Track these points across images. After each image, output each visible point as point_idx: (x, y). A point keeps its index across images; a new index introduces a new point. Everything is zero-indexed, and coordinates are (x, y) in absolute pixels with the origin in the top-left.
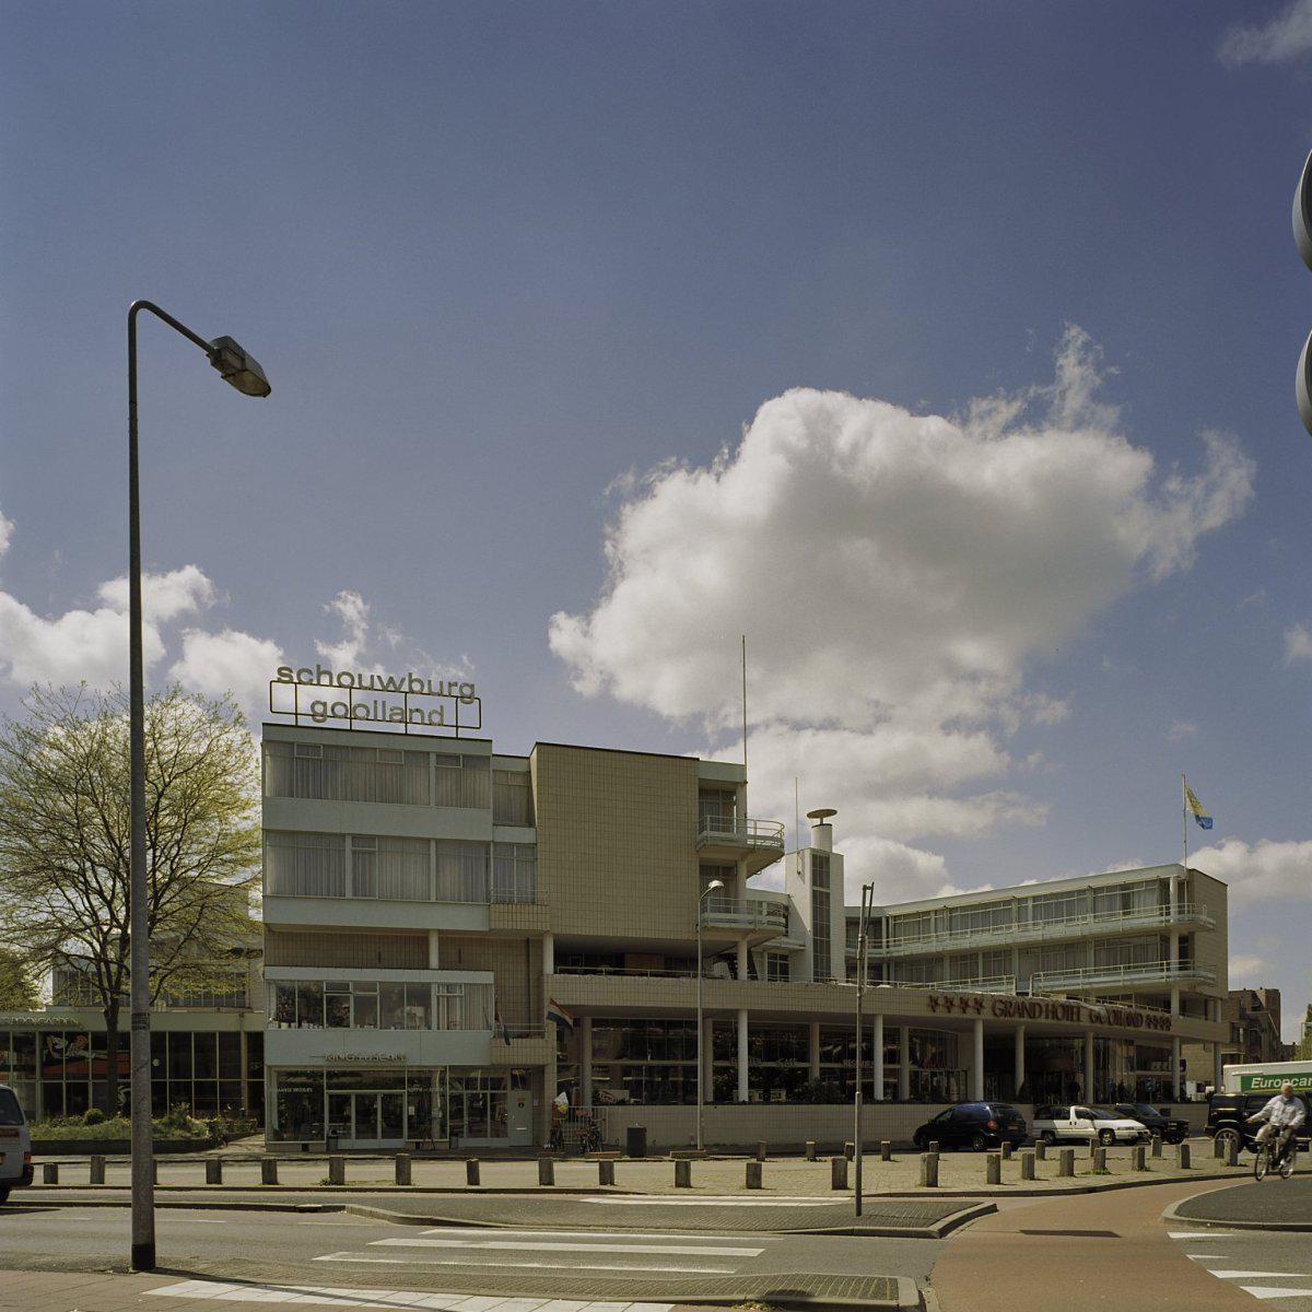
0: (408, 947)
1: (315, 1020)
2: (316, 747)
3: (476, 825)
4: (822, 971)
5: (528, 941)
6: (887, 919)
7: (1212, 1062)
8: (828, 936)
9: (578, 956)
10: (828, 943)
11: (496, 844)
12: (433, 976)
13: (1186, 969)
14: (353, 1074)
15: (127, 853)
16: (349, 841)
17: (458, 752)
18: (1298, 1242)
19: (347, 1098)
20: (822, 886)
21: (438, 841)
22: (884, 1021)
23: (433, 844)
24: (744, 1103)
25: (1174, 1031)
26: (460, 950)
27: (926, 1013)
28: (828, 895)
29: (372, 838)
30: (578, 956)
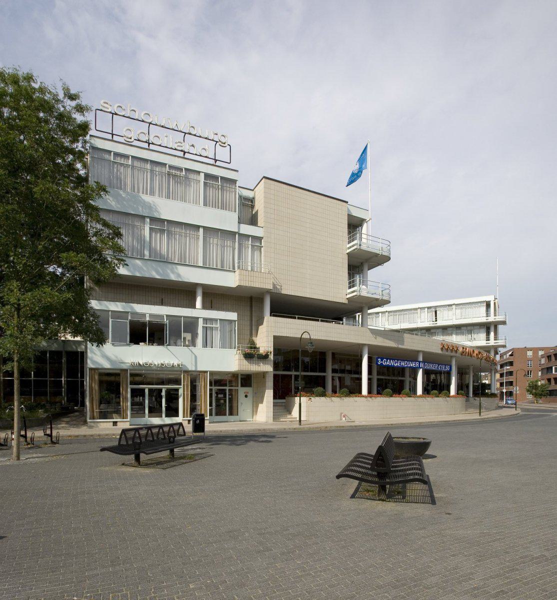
0: (183, 293)
3: (228, 220)
9: (286, 307)
11: (240, 235)
23: (201, 230)
26: (216, 297)
27: (440, 352)
30: (286, 307)
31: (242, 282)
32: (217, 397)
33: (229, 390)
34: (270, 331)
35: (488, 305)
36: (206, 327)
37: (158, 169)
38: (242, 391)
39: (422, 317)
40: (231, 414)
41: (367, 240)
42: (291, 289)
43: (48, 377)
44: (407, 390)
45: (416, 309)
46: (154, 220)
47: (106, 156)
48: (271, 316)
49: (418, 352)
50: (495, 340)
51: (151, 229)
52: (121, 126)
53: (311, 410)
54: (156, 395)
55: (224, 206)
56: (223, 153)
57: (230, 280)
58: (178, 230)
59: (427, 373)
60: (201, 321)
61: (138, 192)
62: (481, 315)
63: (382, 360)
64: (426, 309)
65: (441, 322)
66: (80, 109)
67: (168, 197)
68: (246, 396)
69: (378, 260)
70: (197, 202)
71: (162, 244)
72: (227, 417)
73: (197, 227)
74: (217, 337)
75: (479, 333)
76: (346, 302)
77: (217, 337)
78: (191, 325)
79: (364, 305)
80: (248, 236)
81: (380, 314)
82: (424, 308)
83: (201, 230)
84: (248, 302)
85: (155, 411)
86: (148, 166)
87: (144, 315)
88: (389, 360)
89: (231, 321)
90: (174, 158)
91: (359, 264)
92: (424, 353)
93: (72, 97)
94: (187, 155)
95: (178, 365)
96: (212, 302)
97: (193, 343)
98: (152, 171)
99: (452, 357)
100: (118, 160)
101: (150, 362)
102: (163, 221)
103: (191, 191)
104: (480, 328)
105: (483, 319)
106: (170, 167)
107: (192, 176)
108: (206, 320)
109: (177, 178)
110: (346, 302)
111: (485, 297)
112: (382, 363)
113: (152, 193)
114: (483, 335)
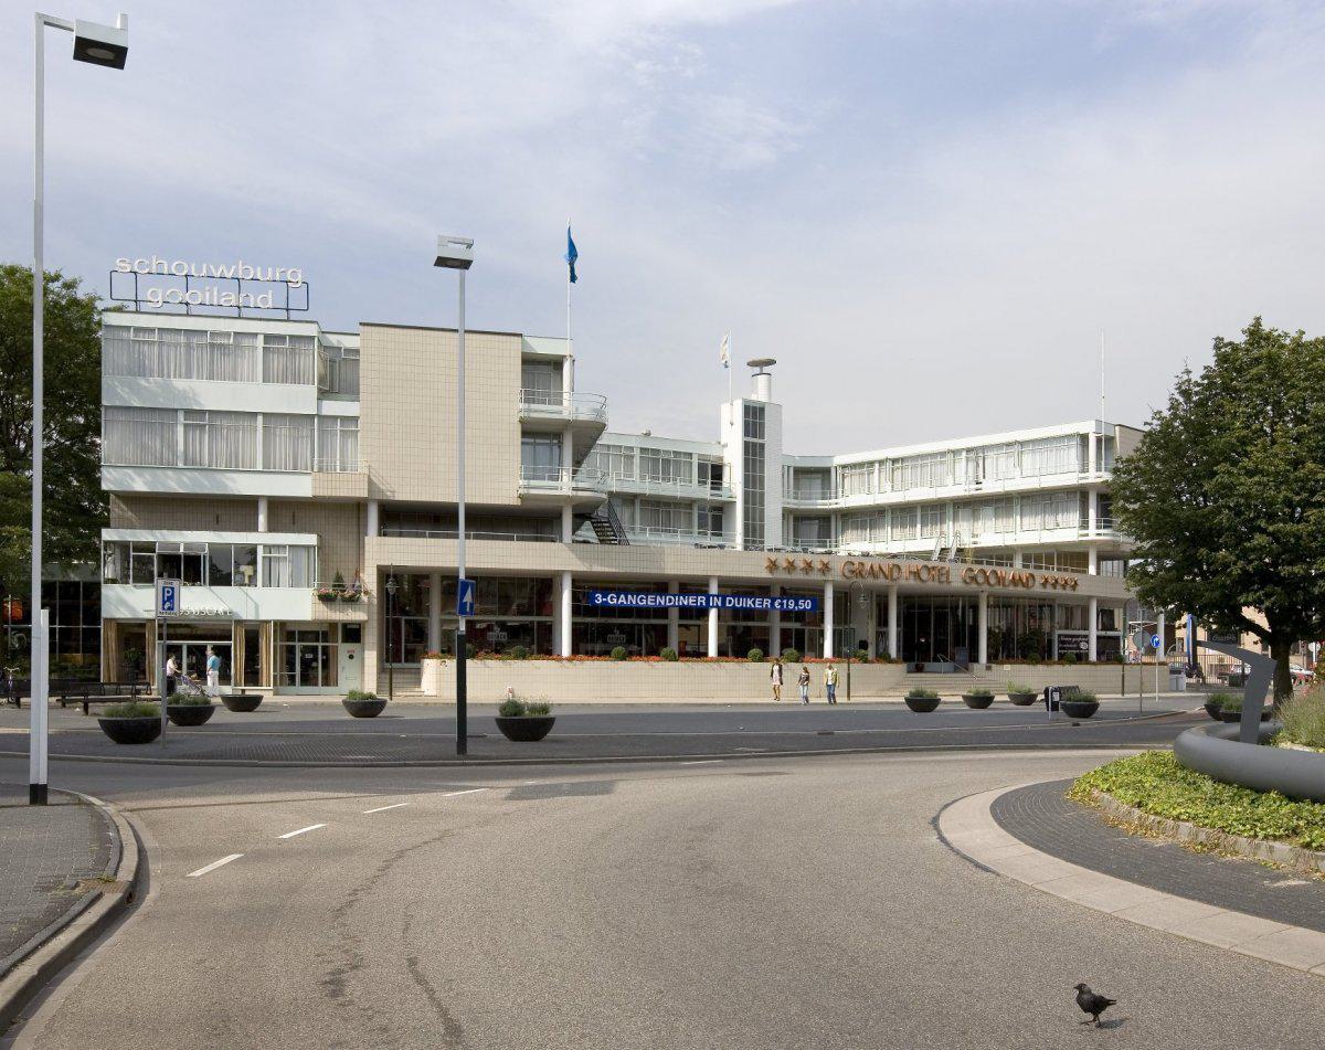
0: (238, 510)
2: (152, 330)
3: (301, 398)
4: (754, 533)
8: (762, 487)
9: (402, 517)
10: (762, 495)
11: (319, 416)
12: (260, 537)
14: (187, 626)
15: (13, 427)
16: (181, 416)
17: (283, 333)
18: (101, 746)
20: (754, 444)
22: (574, 581)
23: (260, 418)
24: (1094, 664)
26: (286, 512)
27: (765, 574)
28: (762, 446)
30: (402, 517)
31: (318, 490)
34: (388, 551)
36: (270, 558)
37: (195, 340)
38: (344, 649)
40: (326, 682)
43: (315, 644)
45: (943, 454)
46: (189, 412)
47: (125, 335)
48: (380, 535)
51: (186, 426)
55: (296, 378)
57: (300, 487)
58: (225, 423)
61: (169, 376)
63: (605, 596)
64: (964, 454)
65: (991, 487)
67: (211, 377)
68: (351, 657)
71: (204, 446)
72: (320, 688)
77: (284, 570)
78: (250, 553)
80: (335, 418)
81: (877, 465)
83: (260, 418)
86: (182, 339)
87: (177, 546)
88: (622, 596)
89: (307, 547)
93: (56, 278)
95: (225, 613)
96: (294, 516)
97: (252, 581)
98: (188, 346)
101: (215, 609)
102: (203, 412)
103: (244, 365)
105: (1071, 479)
106: (213, 334)
107: (246, 342)
108: (269, 548)
109: (218, 353)
112: (607, 602)
113: (189, 376)
114: (1074, 518)
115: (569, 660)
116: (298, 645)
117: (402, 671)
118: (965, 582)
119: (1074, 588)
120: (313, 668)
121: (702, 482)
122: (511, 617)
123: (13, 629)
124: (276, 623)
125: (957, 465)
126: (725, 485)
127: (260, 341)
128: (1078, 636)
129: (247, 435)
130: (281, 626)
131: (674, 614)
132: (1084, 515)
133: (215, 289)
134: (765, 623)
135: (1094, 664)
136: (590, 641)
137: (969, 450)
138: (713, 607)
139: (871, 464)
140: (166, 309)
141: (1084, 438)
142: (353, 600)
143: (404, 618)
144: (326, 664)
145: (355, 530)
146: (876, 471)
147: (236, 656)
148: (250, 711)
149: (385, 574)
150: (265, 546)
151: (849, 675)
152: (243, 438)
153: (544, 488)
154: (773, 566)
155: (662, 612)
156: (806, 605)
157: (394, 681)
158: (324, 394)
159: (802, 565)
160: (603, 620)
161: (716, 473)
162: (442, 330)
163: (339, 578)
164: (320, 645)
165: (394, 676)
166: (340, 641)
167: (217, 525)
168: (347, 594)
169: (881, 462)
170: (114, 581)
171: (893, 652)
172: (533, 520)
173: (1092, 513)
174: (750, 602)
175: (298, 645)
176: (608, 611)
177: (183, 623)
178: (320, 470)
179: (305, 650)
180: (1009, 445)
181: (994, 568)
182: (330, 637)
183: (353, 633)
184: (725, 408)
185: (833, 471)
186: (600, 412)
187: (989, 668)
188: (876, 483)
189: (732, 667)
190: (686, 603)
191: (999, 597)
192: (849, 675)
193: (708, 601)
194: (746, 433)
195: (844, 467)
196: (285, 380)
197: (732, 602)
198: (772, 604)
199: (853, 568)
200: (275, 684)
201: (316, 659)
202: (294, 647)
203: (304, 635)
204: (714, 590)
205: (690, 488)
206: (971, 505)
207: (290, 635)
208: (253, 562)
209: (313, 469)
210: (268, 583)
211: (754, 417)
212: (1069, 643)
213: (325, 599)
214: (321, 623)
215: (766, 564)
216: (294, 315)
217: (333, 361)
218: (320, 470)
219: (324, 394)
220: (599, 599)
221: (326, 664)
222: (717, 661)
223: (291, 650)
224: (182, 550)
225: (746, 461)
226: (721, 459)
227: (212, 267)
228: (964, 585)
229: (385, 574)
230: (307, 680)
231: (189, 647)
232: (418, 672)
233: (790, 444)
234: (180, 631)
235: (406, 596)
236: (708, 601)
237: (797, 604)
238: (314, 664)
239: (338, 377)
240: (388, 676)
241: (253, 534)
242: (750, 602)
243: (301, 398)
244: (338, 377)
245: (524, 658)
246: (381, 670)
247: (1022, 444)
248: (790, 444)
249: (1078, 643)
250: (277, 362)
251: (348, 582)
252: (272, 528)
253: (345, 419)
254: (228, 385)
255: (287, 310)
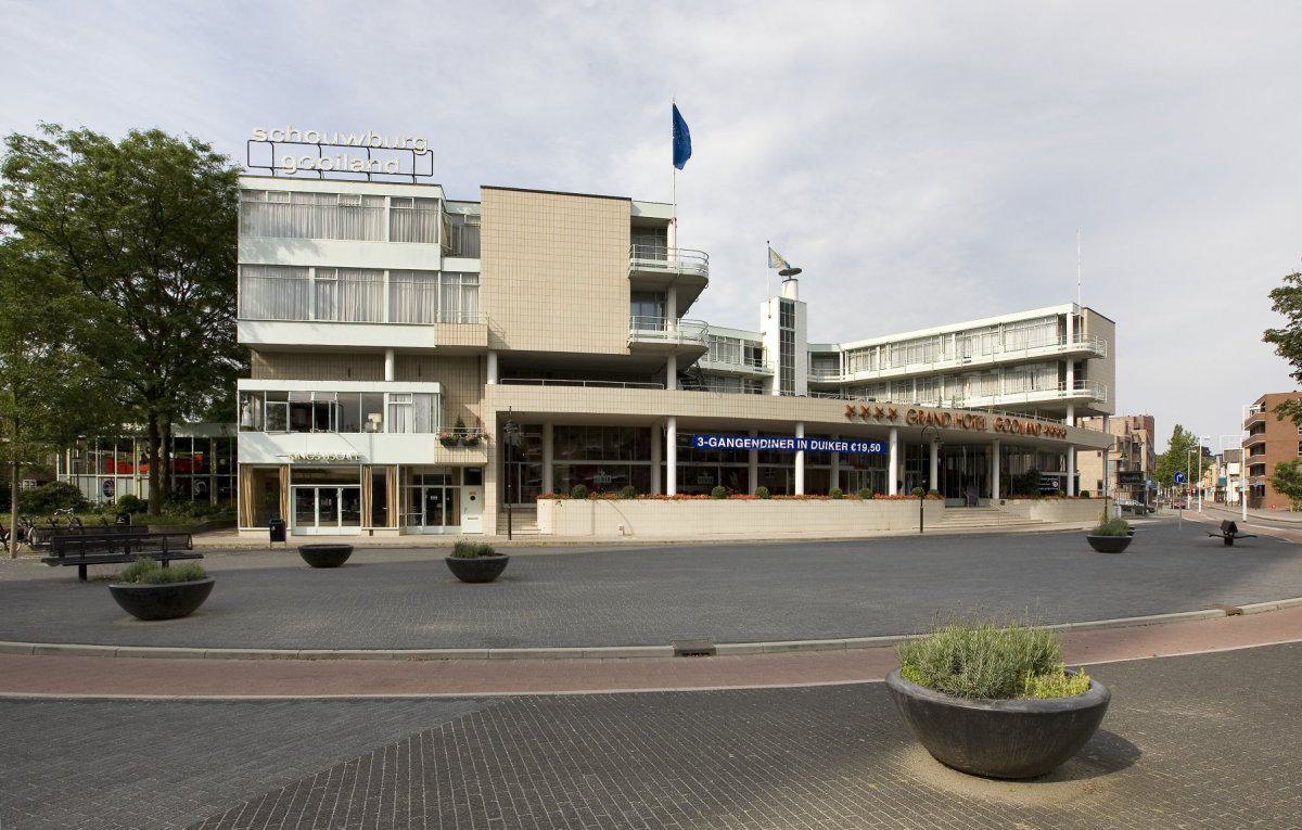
0: (364, 361)
1: (305, 428)
2: (285, 193)
3: (426, 255)
5: (480, 356)
6: (844, 353)
7: (590, 523)
8: (793, 365)
9: (522, 368)
10: (793, 371)
11: (444, 273)
12: (387, 386)
13: (1081, 388)
14: (320, 471)
19: (310, 493)
21: (391, 271)
25: (1068, 439)
26: (412, 362)
27: (845, 420)
28: (793, 333)
29: (331, 269)
30: (522, 368)
32: (428, 500)
33: (447, 489)
35: (1062, 319)
38: (465, 491)
39: (947, 351)
40: (450, 522)
41: (679, 257)
42: (524, 340)
43: (439, 486)
44: (274, 475)
49: (796, 423)
50: (1075, 388)
52: (288, 158)
53: (560, 520)
54: (329, 495)
56: (423, 165)
59: (811, 457)
60: (386, 397)
62: (1051, 342)
63: (706, 439)
65: (978, 359)
66: (214, 158)
67: (341, 237)
68: (473, 498)
69: (689, 288)
70: (380, 238)
73: (381, 271)
74: (408, 415)
75: (1047, 374)
76: (628, 352)
77: (408, 415)
78: (374, 403)
79: (666, 355)
80: (456, 274)
81: (878, 348)
82: (950, 334)
83: (387, 273)
84: (456, 366)
85: (329, 516)
90: (347, 184)
91: (661, 293)
92: (806, 424)
93: (204, 148)
94: (374, 177)
99: (890, 427)
100: (275, 199)
103: (372, 222)
104: (1048, 367)
107: (374, 203)
108: (394, 395)
110: (628, 352)
111: (1054, 308)
114: (1053, 379)
115: (674, 498)
116: (424, 488)
117: (519, 511)
118: (996, 430)
119: (1064, 437)
120: (438, 509)
121: (747, 362)
122: (611, 460)
123: (195, 478)
124: (402, 467)
125: (947, 346)
126: (764, 363)
127: (387, 203)
128: (1051, 477)
129: (375, 289)
130: (407, 470)
131: (754, 457)
132: (1062, 377)
133: (345, 156)
134: (844, 466)
135: (893, 498)
136: (691, 485)
137: (958, 333)
138: (800, 449)
139: (874, 347)
140: (300, 174)
141: (1062, 319)
142: (473, 444)
143: (520, 463)
144: (449, 506)
145: (476, 381)
146: (878, 353)
147: (364, 504)
148: (336, 566)
149: (503, 419)
150: (391, 394)
151: (922, 510)
152: (371, 291)
153: (650, 336)
154: (851, 413)
155: (743, 454)
156: (876, 448)
157: (513, 520)
158: (446, 253)
159: (860, 411)
160: (693, 464)
161: (756, 353)
162: (558, 193)
163: (460, 423)
164: (444, 487)
165: (513, 516)
166: (462, 482)
167: (349, 376)
168: (470, 436)
169: (882, 346)
170: (251, 429)
171: (934, 485)
172: (639, 369)
173: (1070, 375)
174: (831, 445)
175: (424, 488)
176: (713, 455)
177: (317, 467)
178: (444, 322)
179: (430, 492)
180: (994, 327)
181: (1015, 418)
182: (453, 480)
183: (474, 476)
184: (764, 307)
185: (841, 355)
186: (704, 268)
187: (1003, 503)
188: (878, 361)
189: (816, 504)
190: (777, 446)
191: (973, 445)
192: (922, 510)
193: (796, 445)
194: (782, 324)
195: (851, 351)
196: (410, 239)
197: (816, 445)
198: (849, 447)
199: (914, 416)
200: (402, 523)
201: (440, 501)
202: (420, 489)
203: (430, 479)
204: (800, 435)
205: (737, 364)
206: (958, 376)
207: (417, 480)
208: (380, 410)
209: (436, 322)
210: (394, 429)
211: (787, 311)
212: (1045, 482)
213: (447, 443)
214: (446, 467)
215: (845, 411)
216: (420, 180)
217: (456, 228)
218: (444, 322)
219: (446, 253)
220: (701, 442)
221: (449, 506)
222: (805, 499)
223: (417, 493)
224: (312, 399)
225: (782, 345)
226: (761, 344)
227: (342, 136)
228: (994, 432)
229: (503, 419)
230: (433, 520)
231: (321, 491)
232: (534, 511)
233: (816, 332)
234: (314, 476)
235: (522, 434)
236: (796, 445)
237: (869, 447)
238: (439, 506)
239: (460, 237)
240: (507, 515)
241: (380, 383)
242: (831, 445)
243: (426, 255)
244: (460, 237)
245: (634, 498)
246: (500, 510)
247: (1005, 325)
248: (816, 332)
249: (1050, 482)
250: (403, 223)
251: (469, 427)
252: (398, 377)
253: (466, 275)
254: (357, 244)
255: (413, 176)
